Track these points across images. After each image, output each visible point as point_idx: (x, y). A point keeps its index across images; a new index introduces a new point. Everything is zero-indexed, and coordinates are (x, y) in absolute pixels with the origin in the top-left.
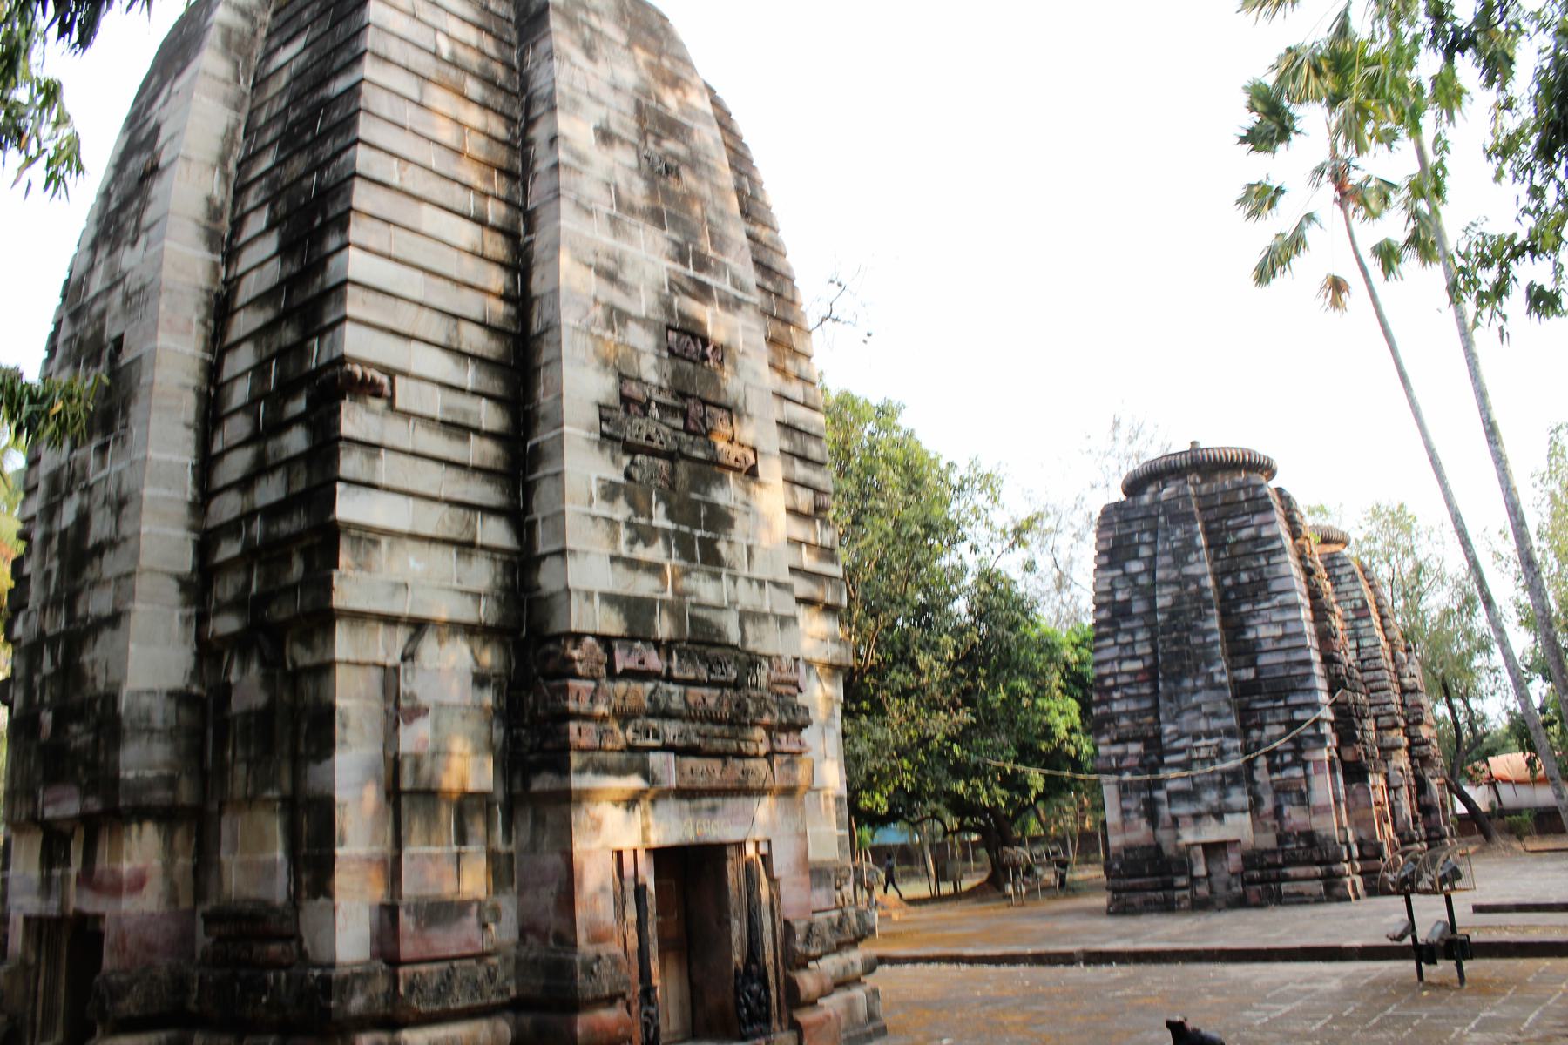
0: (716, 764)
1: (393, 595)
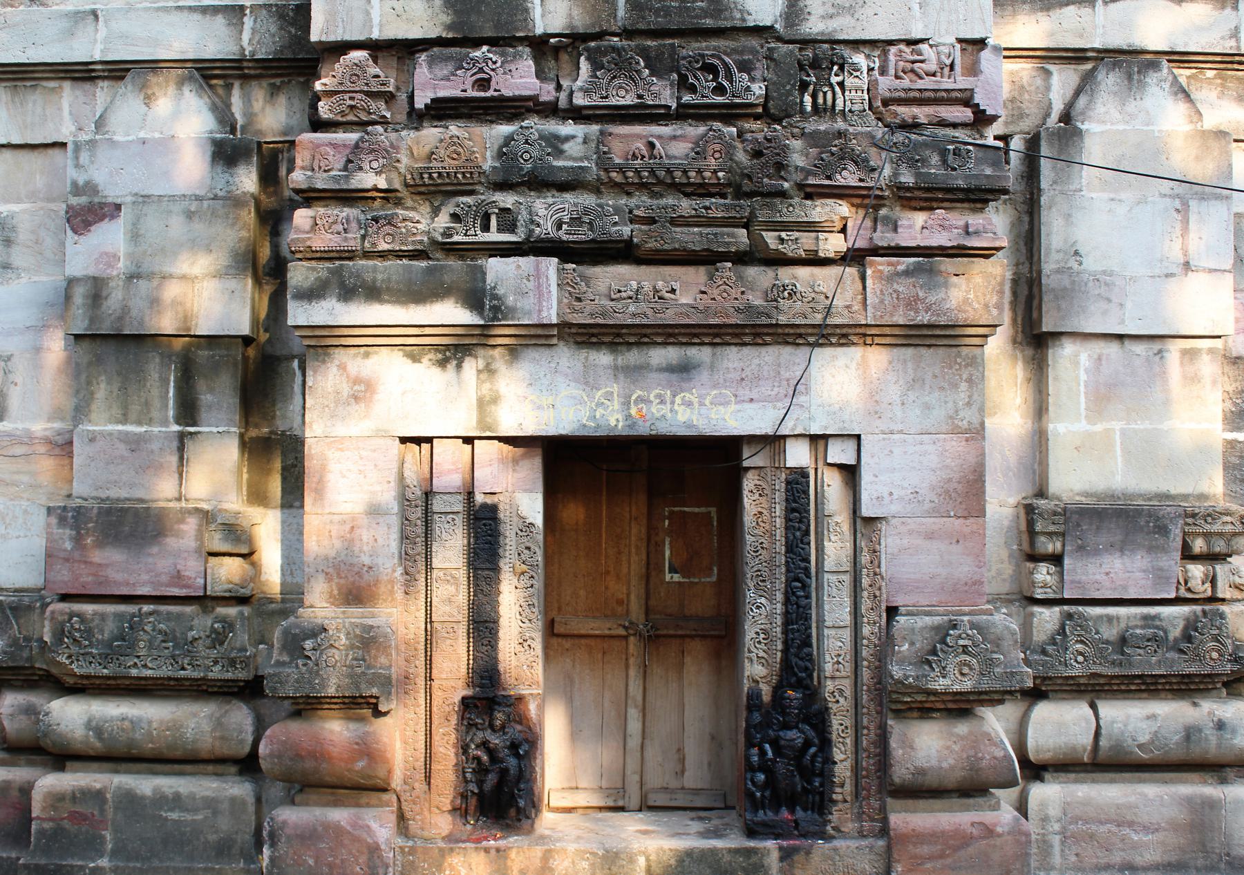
0: (695, 276)
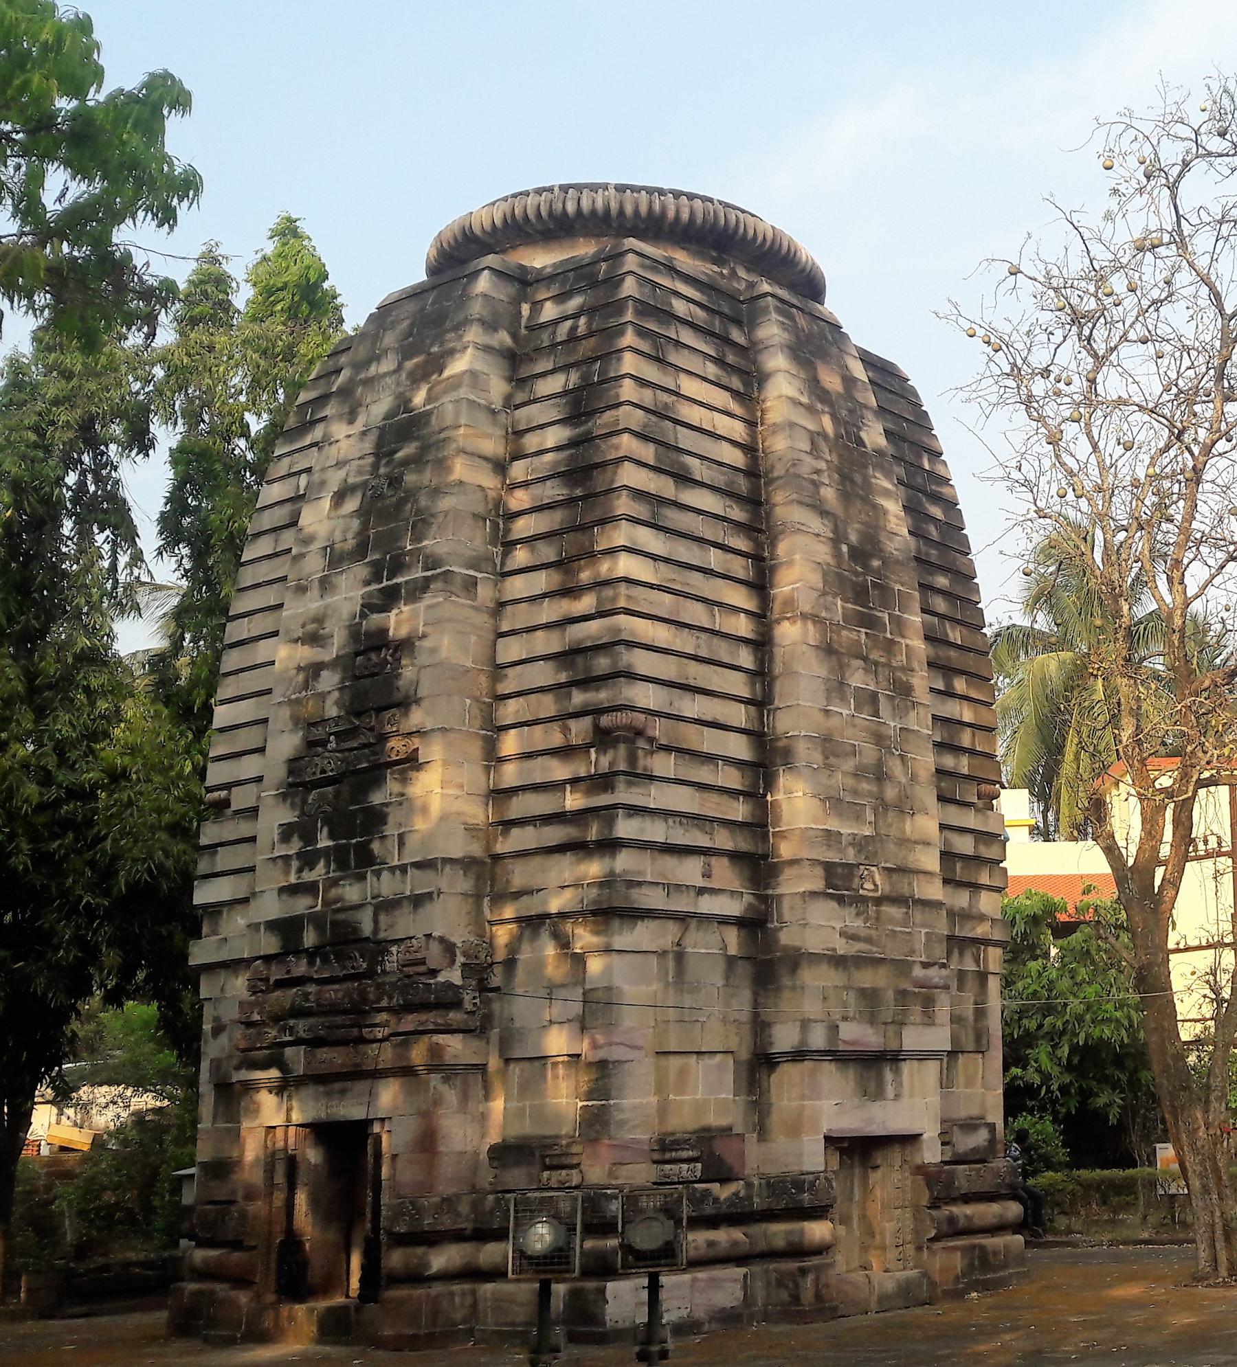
1: (219, 948)
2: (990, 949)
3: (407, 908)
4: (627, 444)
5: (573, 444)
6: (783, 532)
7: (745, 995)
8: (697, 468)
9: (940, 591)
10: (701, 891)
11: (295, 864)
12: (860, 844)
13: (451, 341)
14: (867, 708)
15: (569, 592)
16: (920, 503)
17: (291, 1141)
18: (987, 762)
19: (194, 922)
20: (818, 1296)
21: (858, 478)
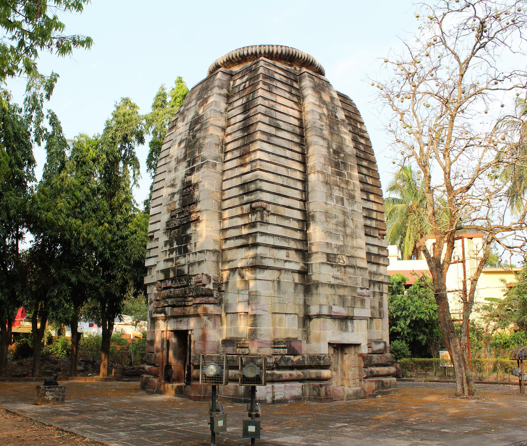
2: (384, 285)
3: (197, 265)
4: (259, 117)
5: (244, 119)
6: (311, 145)
7: (301, 296)
8: (283, 125)
9: (364, 167)
10: (286, 261)
11: (168, 253)
12: (339, 248)
13: (210, 93)
14: (340, 203)
15: (242, 165)
16: (357, 138)
17: (168, 335)
18: (381, 223)
19: (145, 270)
20: (326, 394)
21: (336, 128)
